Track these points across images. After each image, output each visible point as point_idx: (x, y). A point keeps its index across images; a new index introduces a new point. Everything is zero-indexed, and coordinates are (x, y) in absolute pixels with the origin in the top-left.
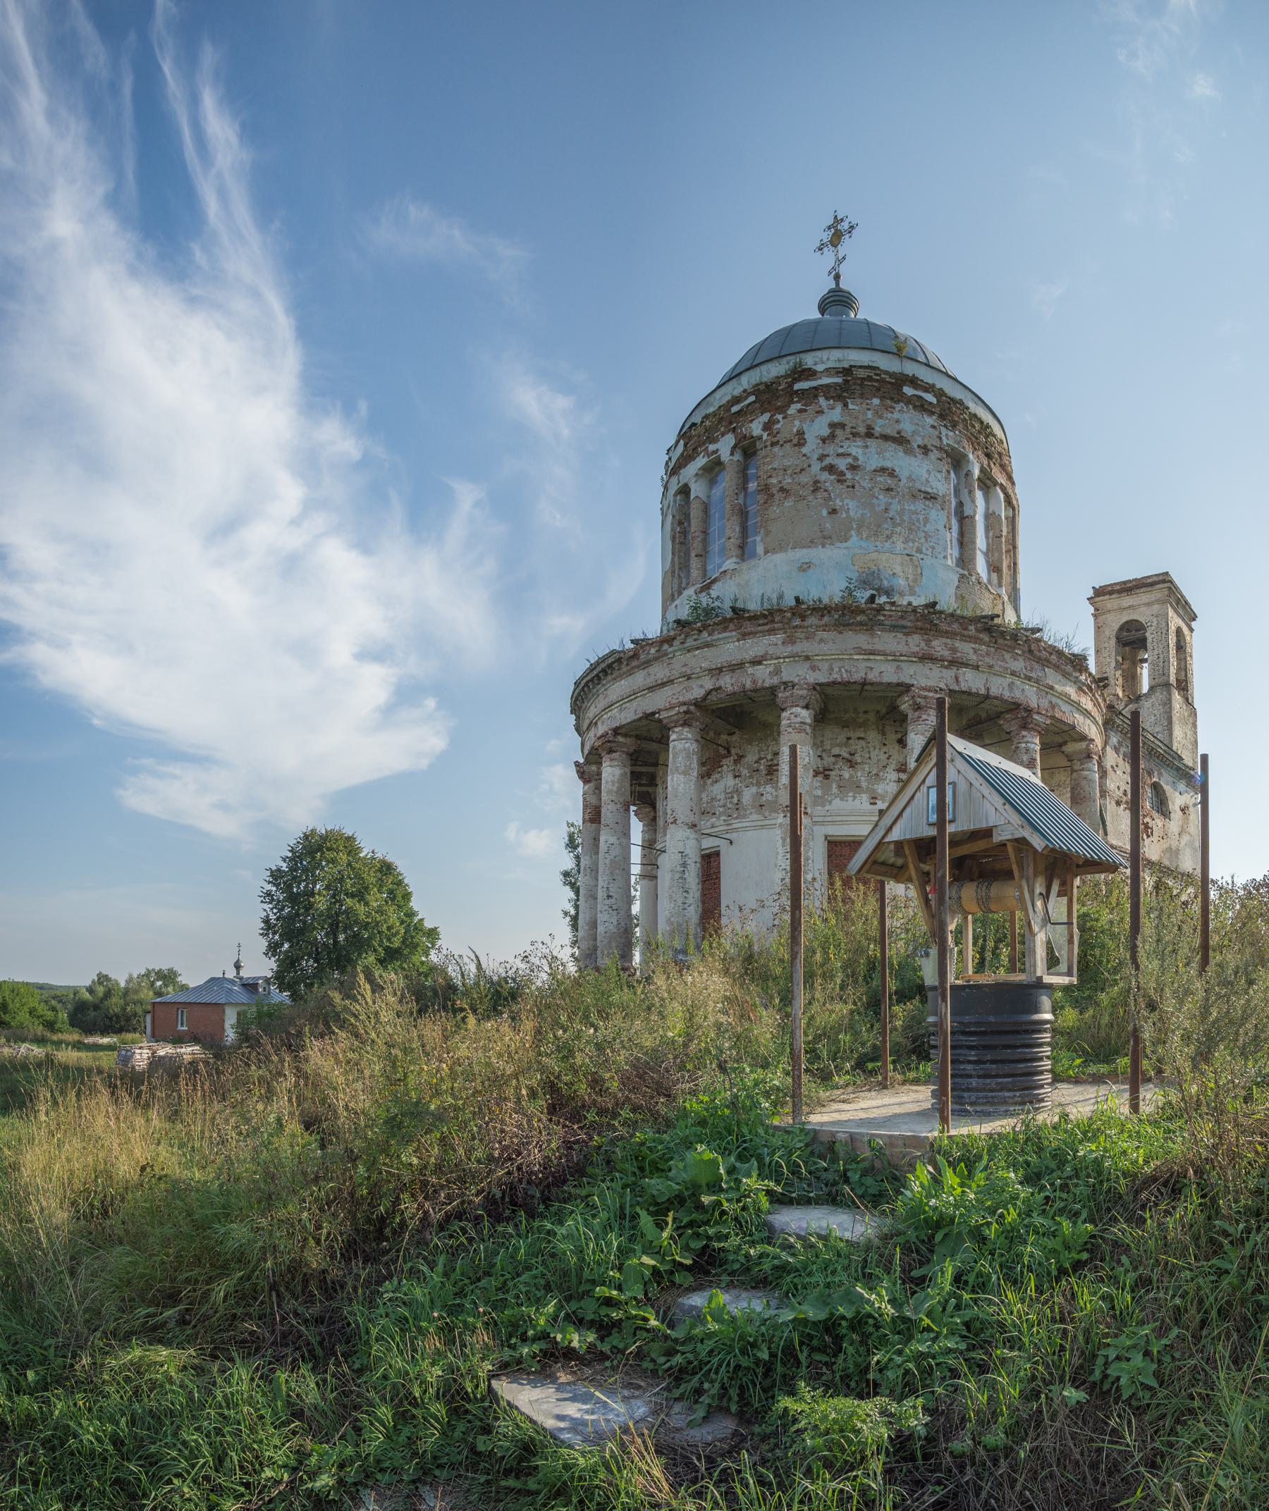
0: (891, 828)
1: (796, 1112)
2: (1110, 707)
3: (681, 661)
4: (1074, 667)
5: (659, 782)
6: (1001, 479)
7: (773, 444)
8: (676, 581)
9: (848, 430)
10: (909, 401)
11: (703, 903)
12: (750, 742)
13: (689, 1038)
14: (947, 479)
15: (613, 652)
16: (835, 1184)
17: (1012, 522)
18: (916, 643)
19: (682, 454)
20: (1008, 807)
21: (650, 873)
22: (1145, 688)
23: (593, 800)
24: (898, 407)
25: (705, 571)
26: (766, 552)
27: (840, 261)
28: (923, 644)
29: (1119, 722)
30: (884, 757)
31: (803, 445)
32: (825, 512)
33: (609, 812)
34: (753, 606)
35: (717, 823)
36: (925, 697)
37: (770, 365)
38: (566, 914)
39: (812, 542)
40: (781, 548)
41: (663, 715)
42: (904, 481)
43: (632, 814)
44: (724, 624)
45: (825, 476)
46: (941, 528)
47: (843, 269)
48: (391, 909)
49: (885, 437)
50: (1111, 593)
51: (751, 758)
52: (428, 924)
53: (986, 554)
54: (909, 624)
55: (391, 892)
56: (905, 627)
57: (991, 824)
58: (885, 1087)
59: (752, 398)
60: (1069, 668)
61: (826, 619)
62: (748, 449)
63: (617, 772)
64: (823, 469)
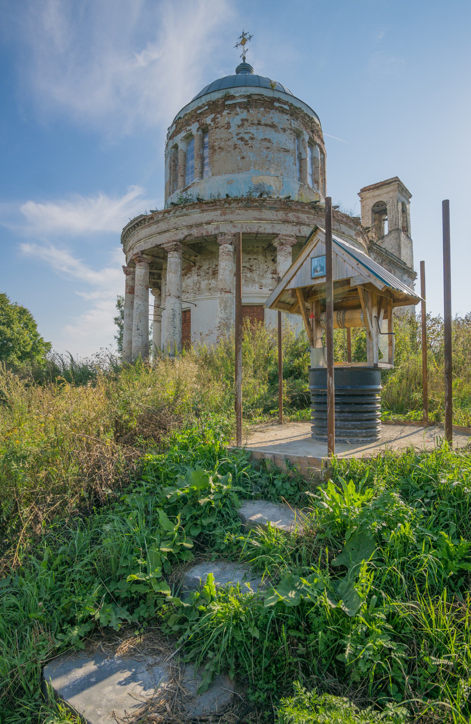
0: (290, 281)
1: (239, 439)
2: (371, 241)
3: (173, 221)
4: (354, 223)
5: (163, 277)
6: (318, 141)
7: (216, 128)
8: (171, 186)
9: (250, 122)
10: (277, 109)
11: (183, 333)
12: (205, 260)
13: (177, 397)
14: (294, 142)
15: (141, 216)
16: (266, 487)
17: (323, 160)
18: (281, 215)
19: (175, 131)
20: (360, 265)
21: (158, 321)
22: (386, 232)
23: (130, 283)
24: (272, 111)
25: (185, 183)
26: (213, 175)
27: (245, 52)
28: (284, 215)
29: (375, 248)
30: (265, 267)
31: (229, 128)
32: (239, 158)
33: (138, 289)
34: (207, 198)
35: (189, 297)
36: (285, 239)
37: (214, 94)
38: (115, 337)
39: (233, 171)
40: (219, 173)
41: (165, 246)
42: (275, 144)
43: (150, 292)
44: (193, 205)
45: (239, 142)
46: (292, 164)
47: (246, 55)
48: (26, 332)
49: (266, 125)
50: (369, 190)
51: (205, 267)
52: (46, 340)
53: (312, 176)
54: (278, 206)
55: (25, 324)
56: (275, 208)
57: (349, 276)
58: (281, 423)
59: (207, 107)
60: (352, 224)
61: (240, 204)
62: (205, 130)
63: (143, 271)
64: (238, 139)
